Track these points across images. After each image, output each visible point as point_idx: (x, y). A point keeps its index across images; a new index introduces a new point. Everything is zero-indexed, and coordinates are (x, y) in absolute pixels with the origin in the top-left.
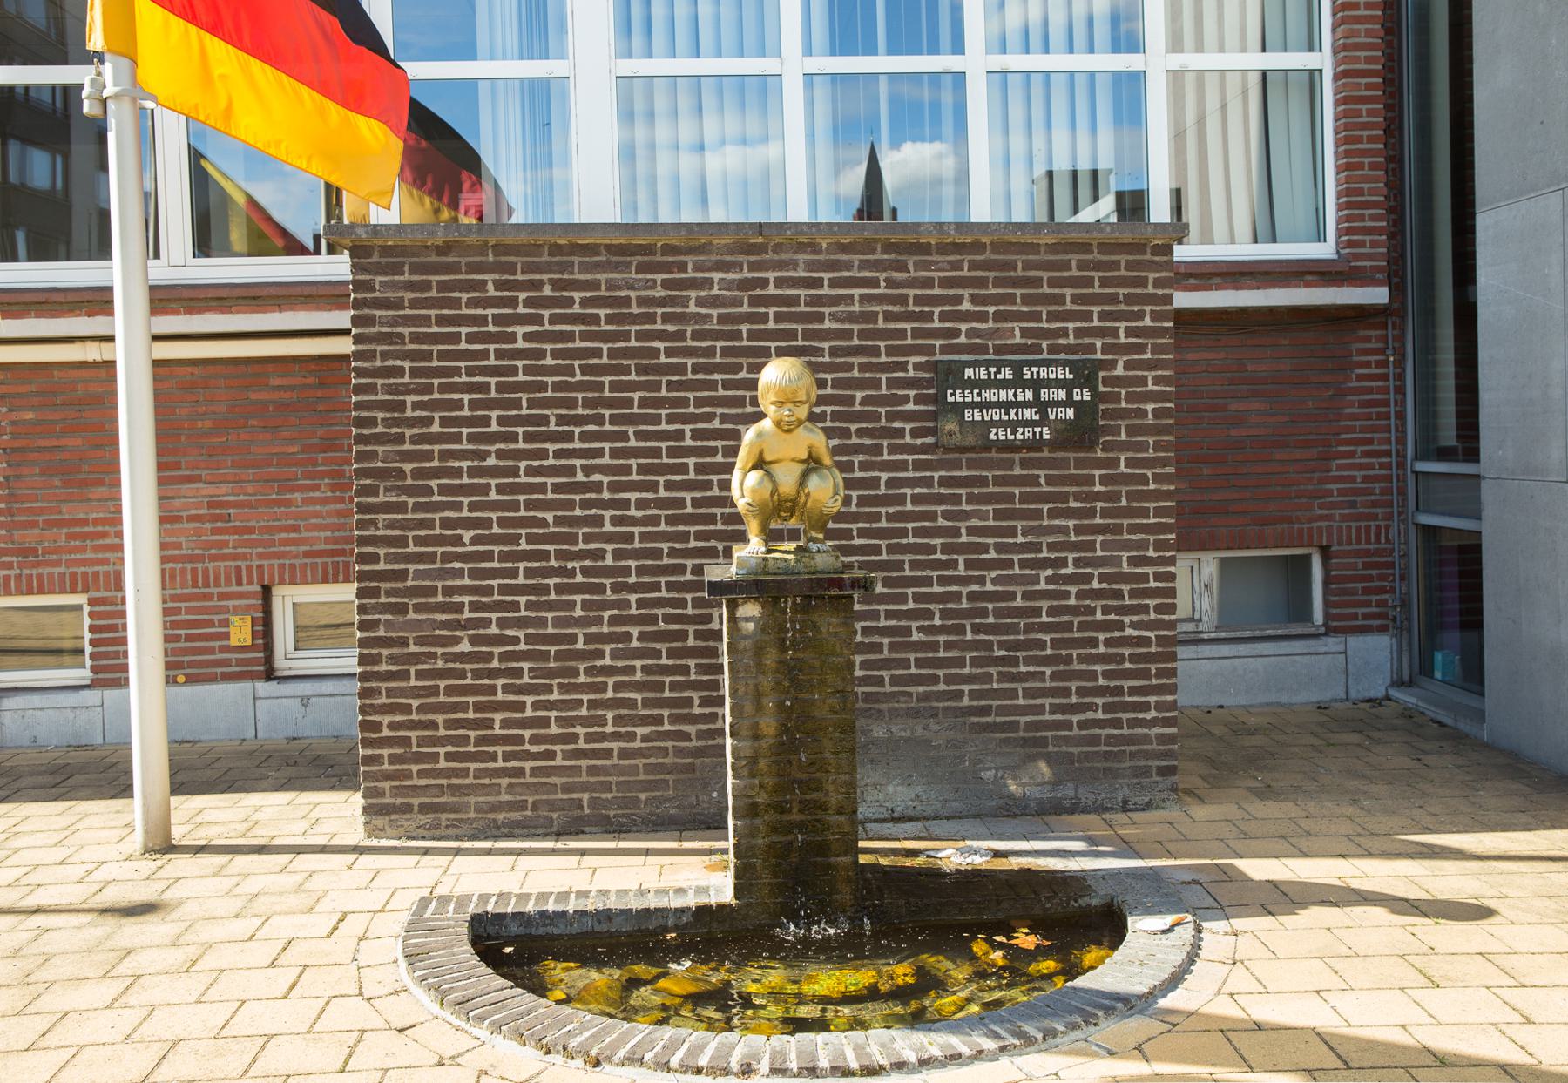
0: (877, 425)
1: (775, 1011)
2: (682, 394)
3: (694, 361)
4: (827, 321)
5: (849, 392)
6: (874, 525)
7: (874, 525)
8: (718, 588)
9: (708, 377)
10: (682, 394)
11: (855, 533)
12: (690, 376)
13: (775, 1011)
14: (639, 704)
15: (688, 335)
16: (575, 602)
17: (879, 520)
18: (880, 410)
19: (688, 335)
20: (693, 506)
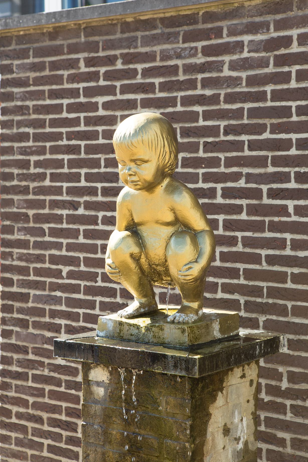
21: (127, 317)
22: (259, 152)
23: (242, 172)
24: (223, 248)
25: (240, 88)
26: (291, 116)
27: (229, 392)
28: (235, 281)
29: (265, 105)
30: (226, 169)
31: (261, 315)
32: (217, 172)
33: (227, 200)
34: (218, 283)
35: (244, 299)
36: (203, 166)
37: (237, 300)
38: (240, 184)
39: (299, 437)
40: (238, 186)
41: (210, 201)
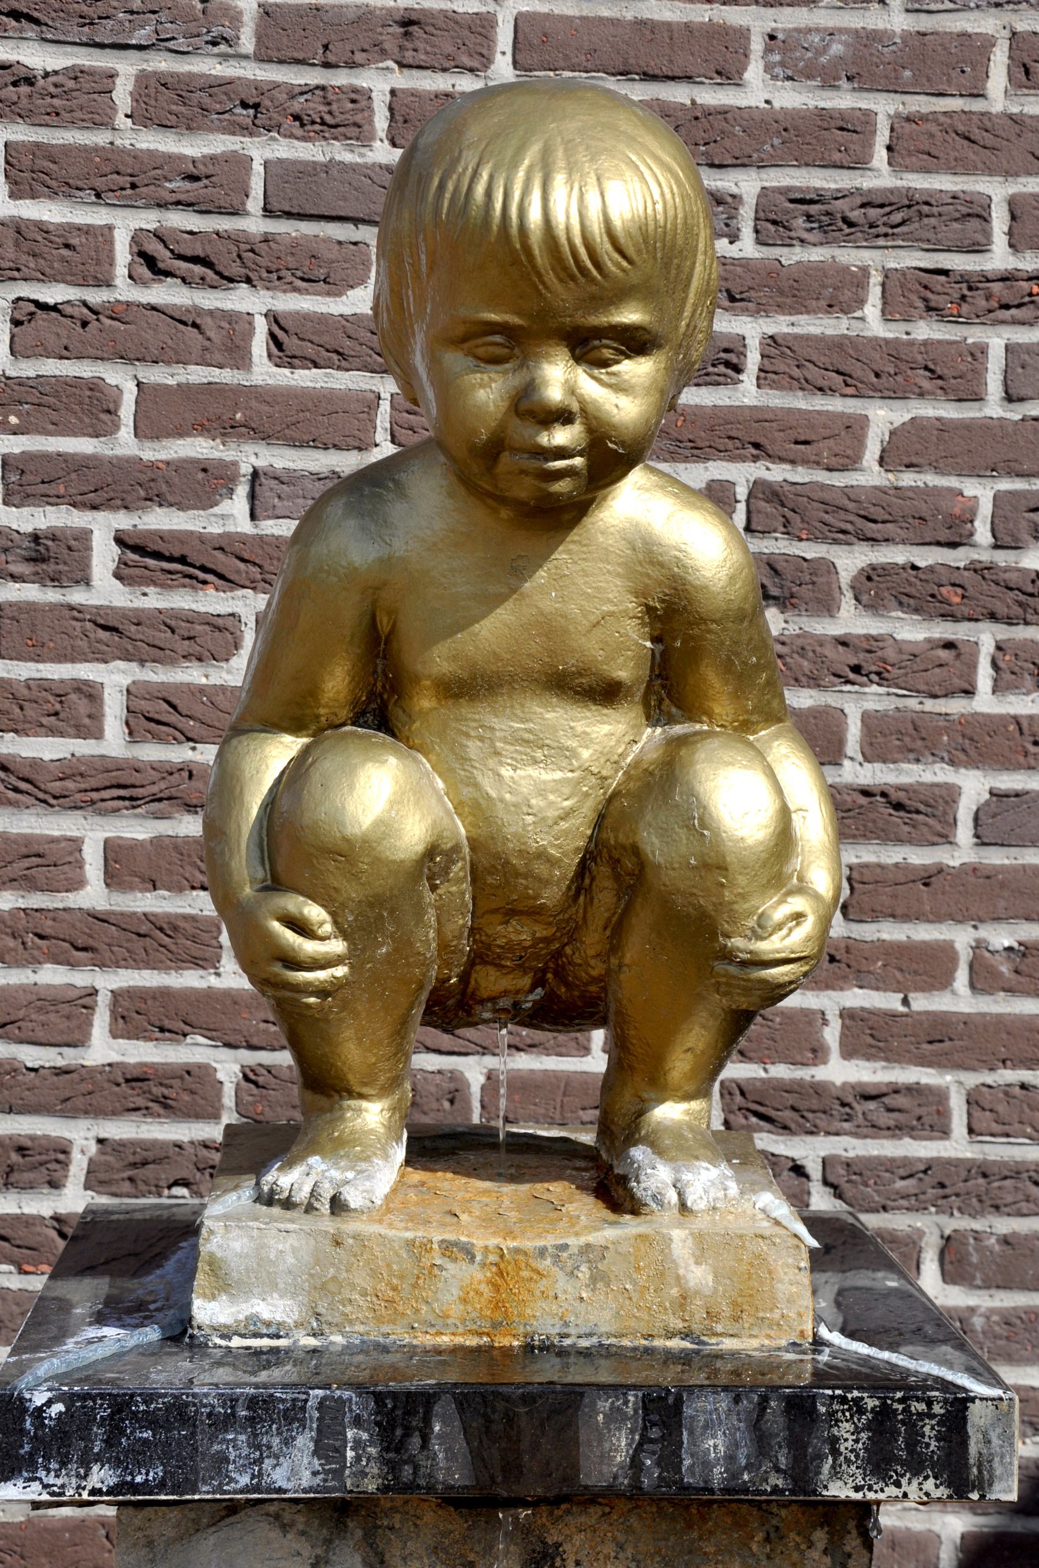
0: (958, 558)
1: (97, 77)
2: (85, 370)
3: (148, 220)
4: (754, 72)
5: (835, 405)
6: (921, 1003)
7: (921, 1003)
8: (579, 1118)
9: (208, 300)
10: (85, 370)
11: (832, 1035)
12: (124, 291)
13: (97, 77)
14: (875, 294)
15: (122, 95)
16: (62, 1151)
17: (942, 981)
18: (971, 488)
19: (122, 95)
20: (112, 879)
21: (384, 624)
22: (326, 375)
23: (235, 464)
24: (124, 822)
25: (225, 57)
26: (77, 884)
27: (151, 1298)
28: (191, 979)
29: (362, 155)
30: (148, 444)
31: (232, 953)
32: (94, 457)
33: (151, 590)
34: (94, 992)
35: (236, 1061)
36: (13, 420)
37: (200, 1066)
38: (223, 517)
39: (52, 596)
40: (216, 529)
41: (52, 596)
